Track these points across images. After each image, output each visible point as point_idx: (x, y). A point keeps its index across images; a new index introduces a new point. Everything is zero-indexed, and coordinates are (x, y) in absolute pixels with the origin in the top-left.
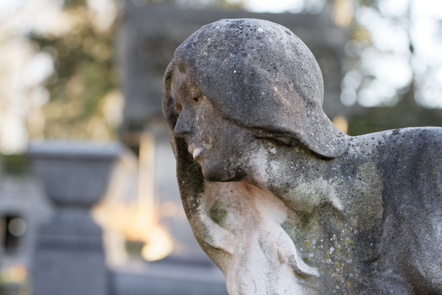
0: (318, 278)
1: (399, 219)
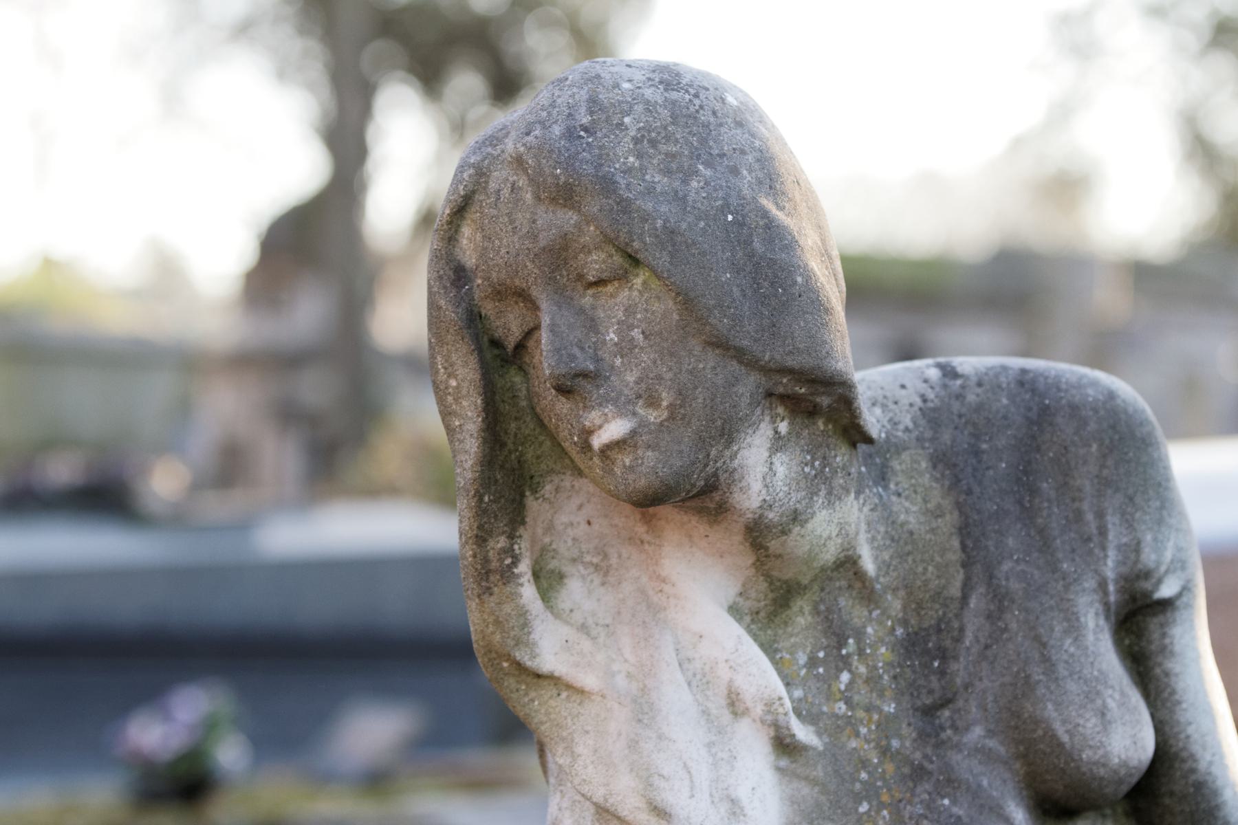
0: (820, 754)
1: (1000, 601)
